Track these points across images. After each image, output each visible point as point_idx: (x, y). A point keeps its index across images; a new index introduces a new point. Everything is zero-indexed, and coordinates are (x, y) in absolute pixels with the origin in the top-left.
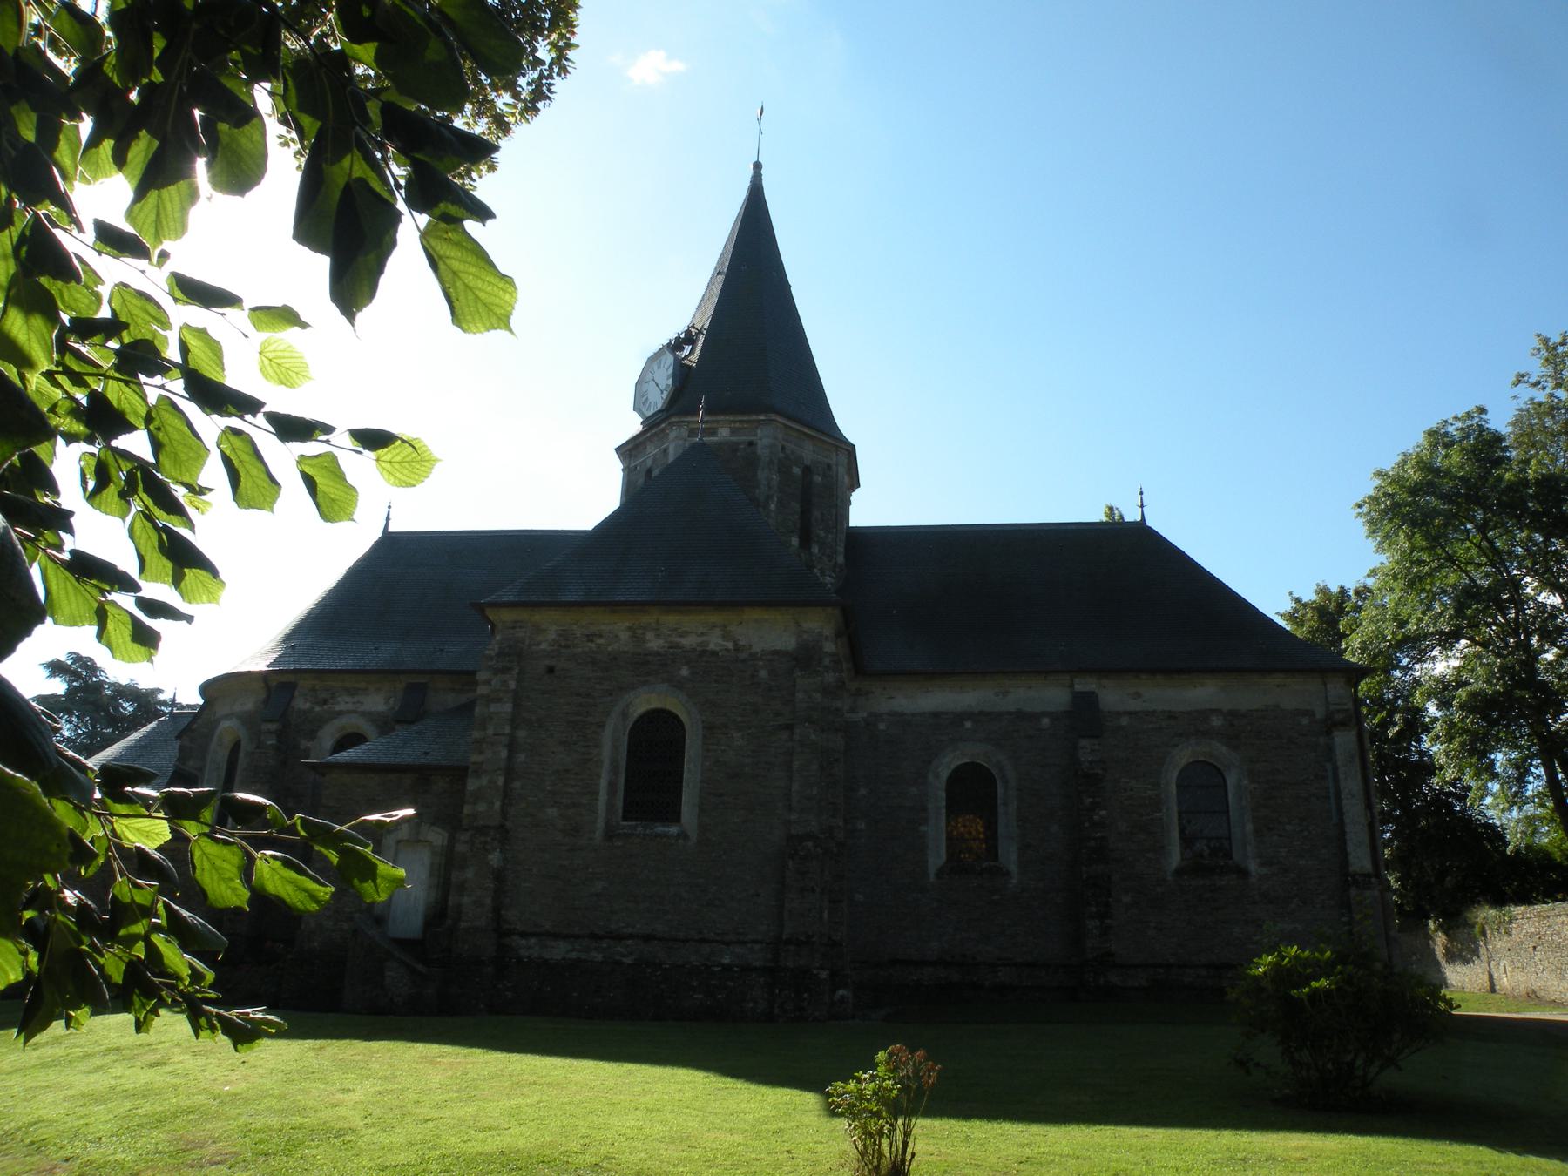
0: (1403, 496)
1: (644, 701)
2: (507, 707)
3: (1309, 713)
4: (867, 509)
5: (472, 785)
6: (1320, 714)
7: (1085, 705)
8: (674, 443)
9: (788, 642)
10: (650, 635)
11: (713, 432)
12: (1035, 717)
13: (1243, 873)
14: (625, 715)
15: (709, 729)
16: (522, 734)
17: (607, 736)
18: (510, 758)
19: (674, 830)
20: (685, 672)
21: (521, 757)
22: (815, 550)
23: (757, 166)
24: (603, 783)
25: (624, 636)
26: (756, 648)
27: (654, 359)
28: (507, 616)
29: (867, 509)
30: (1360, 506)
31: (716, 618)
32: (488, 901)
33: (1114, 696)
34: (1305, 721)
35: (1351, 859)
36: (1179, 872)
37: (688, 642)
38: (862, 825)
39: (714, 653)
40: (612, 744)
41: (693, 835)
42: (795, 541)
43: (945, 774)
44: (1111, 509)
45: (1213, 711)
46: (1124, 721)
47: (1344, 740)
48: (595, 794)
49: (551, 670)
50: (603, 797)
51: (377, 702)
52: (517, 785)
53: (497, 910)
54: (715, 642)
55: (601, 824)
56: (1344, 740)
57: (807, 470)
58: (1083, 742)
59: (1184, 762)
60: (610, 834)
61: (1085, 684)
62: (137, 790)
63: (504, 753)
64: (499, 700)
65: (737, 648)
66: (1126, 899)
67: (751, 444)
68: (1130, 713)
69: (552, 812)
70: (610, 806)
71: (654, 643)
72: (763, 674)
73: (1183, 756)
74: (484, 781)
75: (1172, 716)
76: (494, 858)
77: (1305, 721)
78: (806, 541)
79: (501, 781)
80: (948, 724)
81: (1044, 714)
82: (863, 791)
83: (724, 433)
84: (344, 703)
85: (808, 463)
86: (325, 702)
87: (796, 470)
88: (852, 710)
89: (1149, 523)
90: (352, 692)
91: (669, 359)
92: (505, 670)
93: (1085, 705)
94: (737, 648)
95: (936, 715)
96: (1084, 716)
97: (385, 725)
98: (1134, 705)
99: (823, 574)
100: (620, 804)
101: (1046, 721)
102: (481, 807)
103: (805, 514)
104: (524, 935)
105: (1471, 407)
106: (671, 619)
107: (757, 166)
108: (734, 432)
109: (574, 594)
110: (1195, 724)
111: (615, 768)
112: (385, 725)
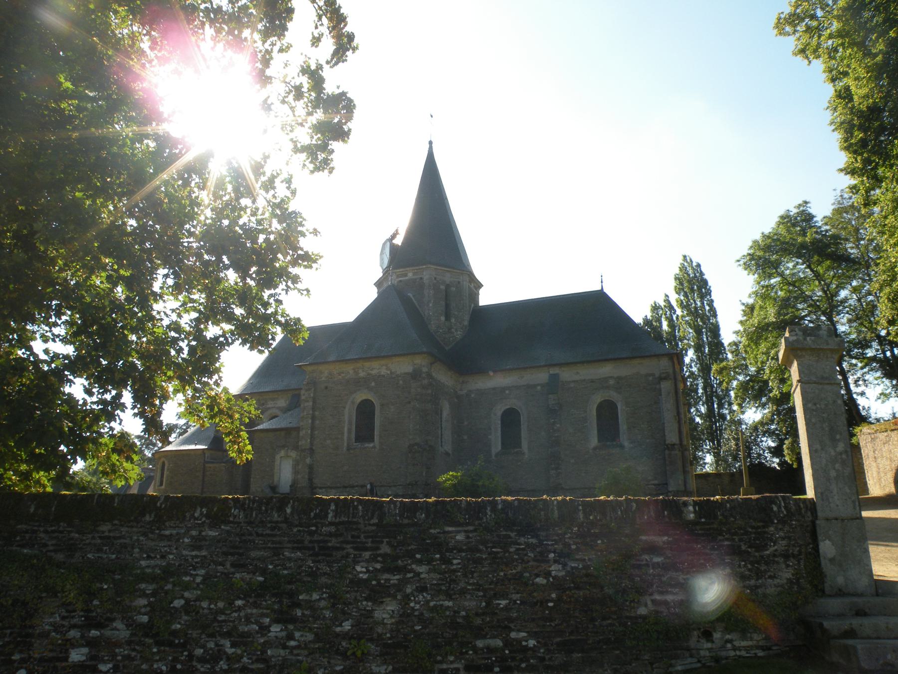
0: (760, 253)
1: (360, 396)
2: (311, 404)
3: (653, 375)
4: (487, 298)
5: (301, 434)
6: (657, 375)
7: (554, 378)
8: (393, 280)
9: (408, 369)
10: (360, 371)
11: (406, 275)
12: (535, 386)
13: (622, 447)
14: (353, 403)
15: (382, 405)
16: (317, 413)
17: (346, 411)
18: (313, 423)
19: (371, 445)
20: (373, 384)
21: (317, 422)
22: (453, 320)
23: (431, 143)
24: (346, 429)
25: (351, 372)
26: (398, 373)
27: (384, 244)
28: (310, 369)
29: (487, 298)
30: (738, 261)
31: (383, 362)
32: (307, 476)
33: (567, 375)
34: (651, 378)
35: (667, 438)
36: (595, 449)
37: (374, 372)
38: (465, 437)
39: (383, 376)
40: (349, 414)
41: (378, 447)
42: (443, 318)
43: (499, 413)
44: (685, 257)
45: (611, 377)
46: (572, 385)
47: (666, 386)
48: (343, 434)
49: (326, 388)
50: (346, 435)
51: (282, 403)
52: (316, 432)
53: (310, 480)
54: (384, 371)
55: (345, 444)
56: (666, 386)
57: (448, 286)
58: (550, 396)
59: (599, 401)
60: (349, 449)
61: (554, 371)
62: (757, 496)
63: (310, 421)
64: (308, 401)
65: (391, 373)
66: (572, 461)
67: (421, 278)
68: (574, 381)
69: (328, 442)
70: (349, 439)
71: (362, 374)
72: (401, 382)
73: (598, 398)
74: (304, 432)
75: (592, 381)
76: (308, 461)
77: (651, 378)
78: (448, 317)
79: (309, 432)
80: (501, 392)
81: (538, 385)
82: (466, 423)
83: (410, 275)
84: (270, 404)
85: (448, 282)
86: (263, 404)
87: (442, 287)
88: (461, 390)
89: (605, 290)
90: (273, 399)
91: (388, 244)
92: (309, 389)
93: (554, 378)
94: (391, 373)
95: (494, 389)
96: (554, 384)
97: (286, 410)
98: (577, 378)
99: (456, 330)
100: (353, 436)
101: (539, 388)
102: (304, 442)
103: (447, 306)
104: (321, 488)
105: (800, 202)
106: (367, 364)
107: (431, 143)
108: (414, 274)
109: (332, 358)
110: (602, 383)
111: (350, 423)
112: (286, 410)
